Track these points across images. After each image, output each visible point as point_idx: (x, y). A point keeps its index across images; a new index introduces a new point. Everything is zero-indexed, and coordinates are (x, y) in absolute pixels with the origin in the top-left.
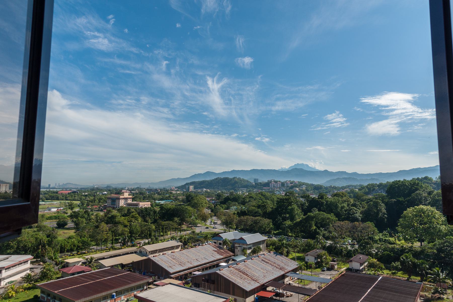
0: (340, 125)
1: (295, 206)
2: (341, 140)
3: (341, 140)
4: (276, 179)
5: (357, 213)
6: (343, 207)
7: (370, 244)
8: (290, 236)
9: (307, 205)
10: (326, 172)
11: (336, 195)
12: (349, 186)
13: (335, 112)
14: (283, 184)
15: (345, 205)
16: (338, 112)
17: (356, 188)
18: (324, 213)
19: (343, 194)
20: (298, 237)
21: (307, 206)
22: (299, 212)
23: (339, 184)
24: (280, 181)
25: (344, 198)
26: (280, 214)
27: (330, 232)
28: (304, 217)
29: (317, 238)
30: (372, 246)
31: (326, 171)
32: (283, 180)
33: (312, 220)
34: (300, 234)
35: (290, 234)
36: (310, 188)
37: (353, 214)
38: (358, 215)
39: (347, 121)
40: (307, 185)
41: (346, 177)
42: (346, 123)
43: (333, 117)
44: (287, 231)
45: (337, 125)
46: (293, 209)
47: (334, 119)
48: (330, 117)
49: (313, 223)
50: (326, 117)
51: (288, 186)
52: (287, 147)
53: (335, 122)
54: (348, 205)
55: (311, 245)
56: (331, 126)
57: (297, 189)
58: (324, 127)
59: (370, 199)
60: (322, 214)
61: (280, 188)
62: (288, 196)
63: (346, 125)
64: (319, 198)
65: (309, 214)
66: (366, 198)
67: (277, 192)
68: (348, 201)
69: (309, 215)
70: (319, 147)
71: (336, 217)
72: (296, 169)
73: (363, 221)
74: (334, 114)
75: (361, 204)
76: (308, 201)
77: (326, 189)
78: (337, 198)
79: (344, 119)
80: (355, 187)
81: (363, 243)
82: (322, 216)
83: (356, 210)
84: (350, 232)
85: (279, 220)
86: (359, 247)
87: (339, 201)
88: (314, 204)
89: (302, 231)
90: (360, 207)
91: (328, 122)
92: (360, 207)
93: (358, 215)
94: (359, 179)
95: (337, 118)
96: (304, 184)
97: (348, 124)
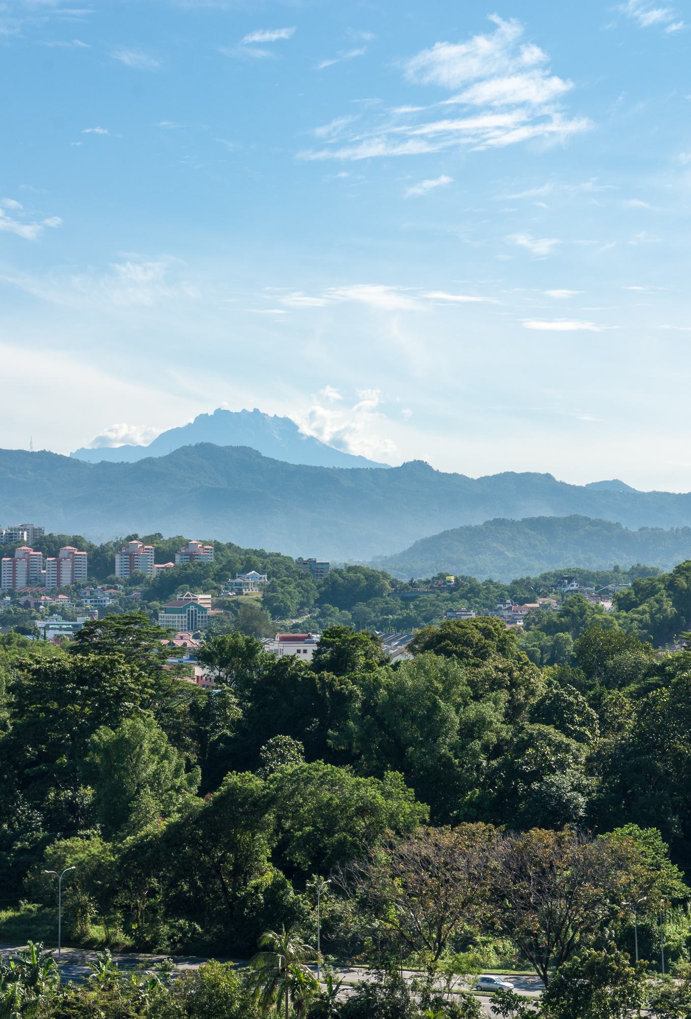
0: (524, 133)
1: (146, 730)
2: (522, 240)
3: (522, 240)
4: (55, 525)
5: (562, 765)
6: (471, 730)
7: (619, 977)
8: (92, 945)
9: (236, 713)
10: (415, 482)
11: (437, 644)
12: (561, 579)
13: (490, 29)
14: (100, 563)
15: (491, 711)
16: (511, 30)
17: (603, 594)
18: (343, 773)
19: (487, 634)
20: (148, 948)
21: (236, 725)
22: (168, 767)
23: (496, 567)
24: (76, 542)
25: (492, 665)
26: (34, 784)
27: (373, 906)
28: (200, 803)
29: (270, 948)
30: (631, 991)
31: (417, 470)
32: (102, 532)
33: (254, 826)
34: (164, 929)
35: (96, 932)
36: (292, 596)
37: (536, 776)
38: (573, 783)
39: (570, 104)
40: (275, 567)
41: (546, 512)
42: (569, 116)
43: (474, 67)
44: (75, 913)
45: (502, 130)
46: (124, 749)
47: (480, 80)
48: (450, 60)
49: (263, 845)
50: (424, 57)
51: (136, 580)
52: (139, 283)
53: (488, 108)
54: (512, 713)
55: (227, 1000)
56: (458, 134)
57: (204, 599)
58: (403, 138)
59: (660, 670)
60: (322, 780)
61: (75, 590)
62: (100, 648)
63: (562, 128)
64: (317, 666)
65: (233, 778)
66: (637, 665)
67: (56, 621)
68: (514, 684)
69: (232, 790)
70: (373, 295)
71: (420, 797)
72: (206, 450)
73: (600, 819)
74: (482, 44)
75: (596, 702)
76: (243, 683)
77: (406, 600)
78: (441, 660)
79: (557, 85)
80: (601, 584)
81: (573, 973)
82: (326, 795)
83: (559, 748)
84: (498, 896)
85: (27, 828)
86: (546, 999)
87: (450, 683)
88: (287, 706)
89: (177, 907)
90: (587, 722)
91: (435, 99)
92: (587, 722)
93: (573, 783)
94: (634, 529)
95: (501, 74)
96: (250, 561)
97: (580, 125)
